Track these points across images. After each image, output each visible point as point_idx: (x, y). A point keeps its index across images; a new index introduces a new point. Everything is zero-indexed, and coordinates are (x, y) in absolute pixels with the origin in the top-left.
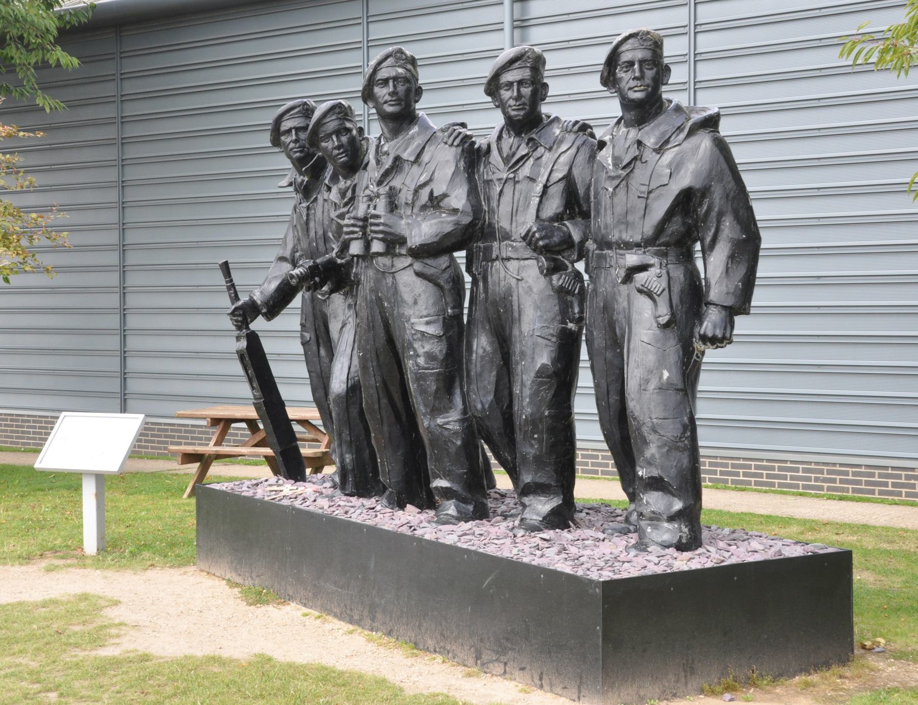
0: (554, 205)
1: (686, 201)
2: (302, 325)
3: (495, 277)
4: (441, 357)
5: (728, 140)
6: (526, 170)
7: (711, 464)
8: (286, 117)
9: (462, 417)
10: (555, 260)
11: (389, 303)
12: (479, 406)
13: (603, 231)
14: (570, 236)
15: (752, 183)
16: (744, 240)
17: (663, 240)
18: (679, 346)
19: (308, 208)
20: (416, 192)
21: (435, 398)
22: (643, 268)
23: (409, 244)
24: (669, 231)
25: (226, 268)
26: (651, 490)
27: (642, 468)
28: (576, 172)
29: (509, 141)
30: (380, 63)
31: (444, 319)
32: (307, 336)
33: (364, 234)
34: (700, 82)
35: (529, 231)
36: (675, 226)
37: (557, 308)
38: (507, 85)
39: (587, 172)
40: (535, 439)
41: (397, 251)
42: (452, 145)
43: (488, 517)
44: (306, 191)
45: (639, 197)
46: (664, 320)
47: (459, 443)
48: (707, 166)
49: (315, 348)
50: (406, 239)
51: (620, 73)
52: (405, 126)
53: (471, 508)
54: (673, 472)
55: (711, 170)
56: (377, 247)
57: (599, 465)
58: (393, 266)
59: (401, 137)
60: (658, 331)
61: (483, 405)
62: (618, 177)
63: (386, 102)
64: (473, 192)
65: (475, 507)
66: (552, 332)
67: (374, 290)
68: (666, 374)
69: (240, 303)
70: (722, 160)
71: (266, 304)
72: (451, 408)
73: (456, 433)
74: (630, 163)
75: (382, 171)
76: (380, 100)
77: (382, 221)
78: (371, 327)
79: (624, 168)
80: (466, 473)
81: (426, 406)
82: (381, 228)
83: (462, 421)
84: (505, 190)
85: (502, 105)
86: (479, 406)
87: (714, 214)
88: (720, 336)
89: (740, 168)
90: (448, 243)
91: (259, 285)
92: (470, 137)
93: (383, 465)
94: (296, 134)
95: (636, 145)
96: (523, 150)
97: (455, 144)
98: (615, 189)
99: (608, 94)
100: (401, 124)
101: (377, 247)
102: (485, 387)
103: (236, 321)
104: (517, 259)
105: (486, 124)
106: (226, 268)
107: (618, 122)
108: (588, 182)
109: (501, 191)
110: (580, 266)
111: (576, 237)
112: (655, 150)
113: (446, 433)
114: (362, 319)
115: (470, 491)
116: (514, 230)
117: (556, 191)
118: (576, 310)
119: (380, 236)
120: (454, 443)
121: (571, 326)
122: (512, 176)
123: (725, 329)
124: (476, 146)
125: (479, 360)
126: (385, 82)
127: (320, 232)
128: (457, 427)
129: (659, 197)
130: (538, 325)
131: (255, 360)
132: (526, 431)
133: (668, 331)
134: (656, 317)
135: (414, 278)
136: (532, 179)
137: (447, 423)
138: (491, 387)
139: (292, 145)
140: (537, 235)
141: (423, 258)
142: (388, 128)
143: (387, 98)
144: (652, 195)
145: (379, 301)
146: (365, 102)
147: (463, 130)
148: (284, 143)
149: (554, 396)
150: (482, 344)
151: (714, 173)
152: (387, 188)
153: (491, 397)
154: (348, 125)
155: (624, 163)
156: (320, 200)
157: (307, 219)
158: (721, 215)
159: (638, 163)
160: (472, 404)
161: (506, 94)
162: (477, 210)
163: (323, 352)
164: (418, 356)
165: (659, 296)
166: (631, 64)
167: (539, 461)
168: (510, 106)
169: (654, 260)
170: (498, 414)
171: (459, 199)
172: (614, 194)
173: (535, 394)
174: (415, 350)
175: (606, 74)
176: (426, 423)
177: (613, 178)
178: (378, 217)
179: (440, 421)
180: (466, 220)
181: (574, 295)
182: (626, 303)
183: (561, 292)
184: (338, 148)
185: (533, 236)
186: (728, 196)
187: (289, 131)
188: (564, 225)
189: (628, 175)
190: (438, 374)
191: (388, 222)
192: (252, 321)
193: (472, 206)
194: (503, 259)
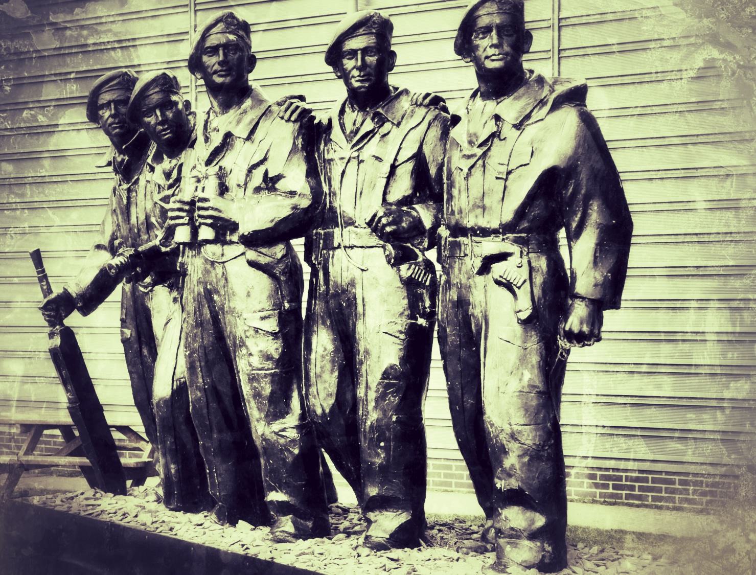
0: (403, 186)
4: (276, 356)
8: (104, 89)
12: (319, 411)
22: (503, 257)
28: (427, 150)
29: (352, 117)
31: (280, 313)
34: (565, 50)
35: (375, 216)
37: (406, 301)
40: (381, 448)
41: (228, 238)
45: (497, 178)
46: (524, 316)
47: (296, 451)
56: (206, 233)
66: (400, 328)
69: (53, 296)
73: (293, 441)
74: (487, 141)
79: (480, 146)
82: (210, 212)
85: (345, 76)
96: (369, 125)
97: (293, 119)
99: (462, 63)
101: (206, 233)
105: (327, 96)
112: (515, 126)
120: (291, 452)
121: (422, 321)
126: (214, 50)
131: (69, 361)
140: (384, 221)
143: (217, 67)
144: (511, 177)
159: (496, 140)
165: (519, 288)
168: (353, 77)
169: (515, 249)
171: (295, 178)
172: (469, 175)
177: (469, 157)
178: (206, 200)
180: (305, 203)
181: (424, 287)
183: (410, 284)
192: (66, 316)
194: (345, 247)
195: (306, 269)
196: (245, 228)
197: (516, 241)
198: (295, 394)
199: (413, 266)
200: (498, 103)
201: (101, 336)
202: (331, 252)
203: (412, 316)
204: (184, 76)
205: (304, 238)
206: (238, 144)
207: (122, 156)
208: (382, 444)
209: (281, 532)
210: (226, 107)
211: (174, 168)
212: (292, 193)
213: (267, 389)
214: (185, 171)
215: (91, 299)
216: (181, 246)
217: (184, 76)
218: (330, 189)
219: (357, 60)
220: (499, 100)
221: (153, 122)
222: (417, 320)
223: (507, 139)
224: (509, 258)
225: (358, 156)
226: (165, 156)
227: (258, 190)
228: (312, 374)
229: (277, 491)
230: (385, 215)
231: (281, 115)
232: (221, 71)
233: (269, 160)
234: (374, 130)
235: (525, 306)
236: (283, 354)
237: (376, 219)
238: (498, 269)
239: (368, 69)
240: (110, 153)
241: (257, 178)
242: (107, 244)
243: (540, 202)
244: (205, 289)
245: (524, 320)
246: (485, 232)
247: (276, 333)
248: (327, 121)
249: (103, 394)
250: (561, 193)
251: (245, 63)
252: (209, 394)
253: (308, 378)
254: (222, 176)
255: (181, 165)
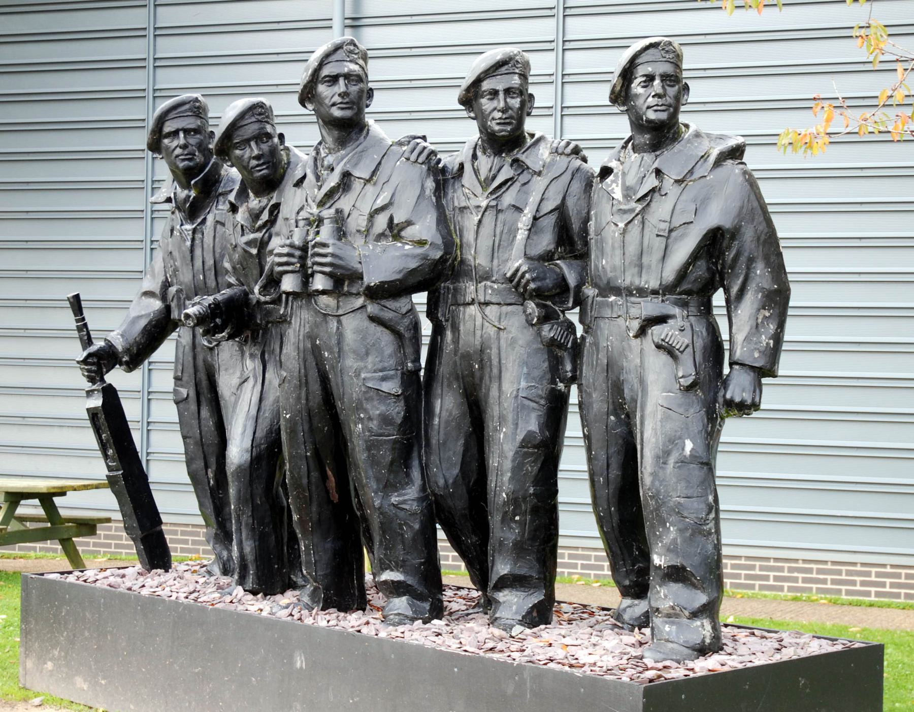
0: (546, 241)
1: (714, 243)
2: (177, 379)
3: (469, 325)
4: (399, 421)
5: (756, 175)
6: (509, 198)
7: (734, 567)
8: (171, 115)
9: (422, 495)
10: (545, 306)
11: (331, 352)
12: (441, 482)
13: (610, 275)
14: (564, 279)
15: (784, 227)
16: (776, 290)
17: (685, 286)
18: (703, 412)
19: (194, 231)
20: (372, 215)
21: (390, 471)
22: (662, 320)
23: (366, 280)
24: (692, 277)
25: (76, 304)
26: (669, 581)
27: (660, 555)
28: (570, 202)
29: (485, 163)
30: (327, 55)
31: (403, 374)
32: (184, 392)
33: (304, 266)
34: (568, 107)
35: (517, 270)
36: (700, 270)
37: (546, 364)
38: (490, 93)
39: (583, 203)
40: (516, 522)
41: (346, 289)
42: (416, 161)
43: (364, 610)
44: (193, 211)
45: (658, 236)
46: (686, 382)
47: (417, 526)
48: (737, 204)
49: (193, 407)
50: (362, 274)
51: (637, 88)
52: (353, 135)
53: (427, 606)
54: (697, 560)
55: (742, 208)
56: (319, 283)
57: (859, 574)
58: (338, 307)
59: (348, 149)
60: (679, 394)
61: (446, 481)
62: (633, 210)
63: (334, 105)
64: (443, 221)
65: (431, 605)
66: (540, 392)
67: (311, 337)
68: (689, 446)
69: (93, 349)
70: (753, 197)
71: (127, 351)
72: (407, 484)
73: (413, 514)
74: (646, 195)
75: (325, 189)
76: (327, 101)
77: (329, 250)
78: (304, 382)
79: (639, 200)
80: (422, 564)
81: (378, 480)
82: (328, 260)
83: (420, 500)
84: (484, 221)
85: (481, 118)
86: (441, 482)
87: (743, 259)
88: (749, 402)
89: (770, 209)
90: (412, 281)
91: (114, 328)
92: (433, 153)
93: (308, 554)
94: (185, 137)
95: (654, 174)
96: (507, 172)
97: (420, 160)
98: (626, 225)
99: (465, 114)
100: (350, 133)
101: (319, 283)
102: (449, 458)
103: (88, 371)
104: (499, 304)
105: (457, 137)
106: (76, 304)
107: (624, 147)
108: (584, 215)
109: (480, 221)
110: (573, 316)
111: (572, 280)
112: (677, 181)
113: (401, 514)
114: (290, 371)
115: (426, 586)
116: (495, 269)
117: (549, 223)
118: (569, 367)
119: (327, 269)
120: (411, 527)
121: (561, 386)
122: (493, 203)
123: (754, 391)
124: (440, 165)
125: (442, 426)
126: (333, 79)
127: (210, 262)
128: (415, 506)
129: (683, 236)
130: (523, 384)
132: (506, 512)
133: (691, 395)
134: (677, 378)
135: (367, 323)
136: (519, 210)
137: (404, 502)
138: (457, 459)
139: (178, 151)
140: (527, 276)
141: (381, 299)
142: (333, 137)
143: (337, 99)
144: (674, 234)
145: (316, 351)
146: (302, 102)
147: (424, 144)
148: (167, 148)
149: (540, 470)
150: (446, 405)
151: (744, 210)
152: (332, 211)
153: (456, 471)
154: (269, 129)
155: (639, 195)
156: (210, 219)
157: (192, 245)
158: (751, 261)
159: (656, 195)
160: (432, 480)
161: (486, 104)
162: (449, 244)
163: (205, 413)
164: (370, 419)
165: (682, 352)
166: (650, 78)
167: (519, 550)
168: (493, 119)
169: (676, 311)
170: (463, 491)
171: (425, 227)
172: (625, 231)
173: (517, 469)
174: (365, 411)
175: (618, 88)
176: (377, 503)
177: (625, 212)
178: (324, 245)
179: (394, 499)
180: (438, 254)
181: (566, 349)
182: (639, 361)
183: (552, 346)
184: (257, 158)
185: (523, 276)
186: (758, 239)
187: (175, 133)
188: (556, 265)
189: (643, 209)
190: (395, 442)
191: (338, 252)
192: (107, 372)
193: (443, 238)
194: (480, 304)
195: (427, 328)
196: (372, 278)
197: (677, 303)
198: (415, 463)
199: (555, 326)
200: (657, 156)
201: (152, 398)
202: (461, 308)
203: (553, 382)
204: (286, 106)
205: (425, 294)
206: (357, 185)
207: (186, 192)
208: (517, 518)
209: (396, 614)
210: (342, 143)
211: (264, 209)
212: (421, 243)
213: (386, 455)
214: (284, 211)
215: (138, 353)
216: (284, 296)
217: (286, 106)
218: (461, 241)
219: (499, 101)
220: (658, 153)
221: (247, 156)
222: (556, 385)
223: (669, 195)
224: (669, 321)
225: (497, 205)
226: (251, 194)
227: (381, 236)
228: (434, 441)
229: (392, 570)
230: (529, 270)
231: (406, 155)
232: (341, 103)
233: (395, 205)
234: (512, 178)
235: (687, 370)
236: (405, 418)
237: (519, 274)
238: (657, 332)
239: (510, 112)
240: (169, 187)
241: (381, 222)
242: (158, 291)
243: (702, 264)
244: (314, 345)
245: (687, 387)
246: (642, 292)
247: (398, 396)
248: (456, 167)
249: (493, 462)
250: (724, 254)
251: (365, 95)
252: (311, 461)
253: (428, 444)
254: (340, 220)
255: (277, 206)
